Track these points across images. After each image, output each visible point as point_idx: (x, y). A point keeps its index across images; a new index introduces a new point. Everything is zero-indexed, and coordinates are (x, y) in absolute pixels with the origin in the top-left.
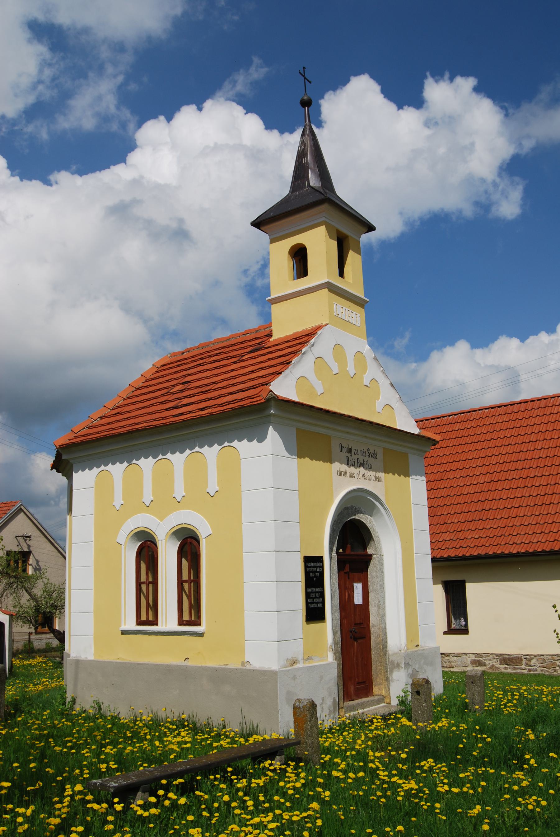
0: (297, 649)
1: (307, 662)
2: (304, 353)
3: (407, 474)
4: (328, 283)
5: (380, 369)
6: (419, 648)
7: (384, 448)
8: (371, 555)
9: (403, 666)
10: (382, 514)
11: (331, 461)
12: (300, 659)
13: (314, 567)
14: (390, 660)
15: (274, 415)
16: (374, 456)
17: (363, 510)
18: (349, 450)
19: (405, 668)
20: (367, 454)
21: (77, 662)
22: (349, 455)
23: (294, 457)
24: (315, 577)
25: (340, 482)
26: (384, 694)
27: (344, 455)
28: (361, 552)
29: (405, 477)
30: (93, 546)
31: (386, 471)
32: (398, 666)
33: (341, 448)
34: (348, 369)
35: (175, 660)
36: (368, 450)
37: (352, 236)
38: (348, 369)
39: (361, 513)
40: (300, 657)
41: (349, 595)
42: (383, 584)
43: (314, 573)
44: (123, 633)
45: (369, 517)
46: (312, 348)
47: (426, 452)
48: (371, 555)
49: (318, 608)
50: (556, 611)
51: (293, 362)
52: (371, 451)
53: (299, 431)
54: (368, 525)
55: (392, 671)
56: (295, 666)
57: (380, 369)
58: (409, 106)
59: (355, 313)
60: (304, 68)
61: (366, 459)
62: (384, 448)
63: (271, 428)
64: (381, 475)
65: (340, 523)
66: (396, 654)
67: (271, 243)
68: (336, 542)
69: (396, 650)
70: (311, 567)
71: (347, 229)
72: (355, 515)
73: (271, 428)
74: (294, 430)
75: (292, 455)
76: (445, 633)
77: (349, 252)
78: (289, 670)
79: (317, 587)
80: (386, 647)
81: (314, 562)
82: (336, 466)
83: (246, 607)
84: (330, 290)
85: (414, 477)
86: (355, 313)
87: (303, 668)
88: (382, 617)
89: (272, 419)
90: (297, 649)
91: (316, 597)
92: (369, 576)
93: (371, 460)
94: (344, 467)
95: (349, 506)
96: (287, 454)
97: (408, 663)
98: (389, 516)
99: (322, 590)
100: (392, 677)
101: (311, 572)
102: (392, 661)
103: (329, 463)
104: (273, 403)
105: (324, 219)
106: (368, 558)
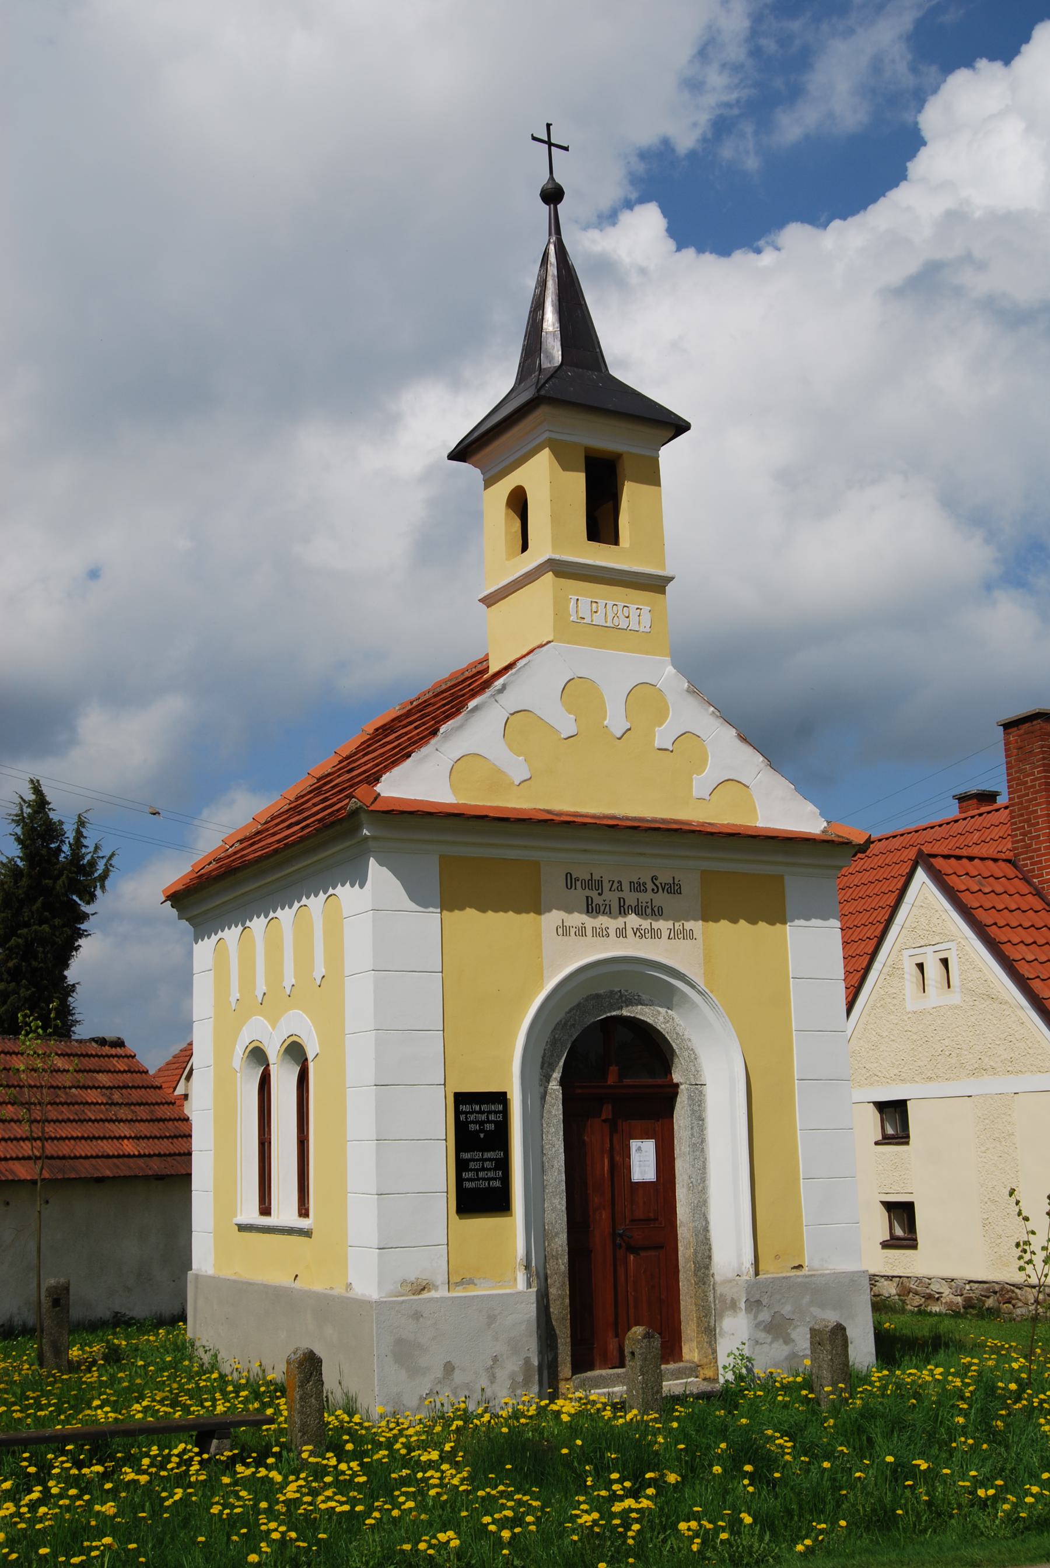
0: (432, 1263)
1: (461, 1288)
2: (476, 708)
3: (778, 916)
4: (550, 561)
5: (707, 710)
6: (805, 1271)
7: (703, 872)
8: (677, 1085)
9: (743, 1306)
10: (693, 1003)
11: (538, 908)
12: (439, 1283)
13: (481, 1112)
14: (718, 1292)
15: (374, 838)
16: (673, 888)
17: (644, 997)
18: (596, 885)
19: (748, 1309)
20: (650, 886)
21: (197, 1276)
22: (594, 894)
23: (431, 909)
24: (481, 1131)
25: (562, 948)
26: (696, 1360)
27: (580, 894)
28: (659, 1081)
29: (772, 923)
30: (212, 1074)
31: (707, 916)
32: (734, 1306)
33: (571, 881)
34: (606, 723)
35: (280, 1278)
36: (654, 879)
37: (634, 450)
38: (606, 723)
39: (640, 1002)
40: (441, 1278)
41: (612, 1164)
42: (703, 1141)
43: (482, 1123)
44: (242, 1228)
45: (663, 1010)
46: (499, 697)
47: (841, 868)
48: (677, 1085)
49: (490, 1190)
50: (1018, 1203)
51: (441, 731)
52: (664, 878)
53: (447, 864)
54: (661, 1026)
55: (722, 1317)
56: (425, 1295)
57: (707, 710)
58: (992, 59)
59: (633, 607)
60: (548, 126)
61: (644, 897)
62: (703, 872)
63: (372, 860)
64: (696, 926)
65: (573, 1026)
66: (730, 1281)
67: (486, 488)
68: (561, 1063)
69: (731, 1275)
70: (472, 1113)
71: (606, 438)
72: (621, 1008)
73: (372, 861)
74: (436, 858)
75: (426, 907)
76: (885, 1245)
77: (623, 485)
78: (403, 1302)
79: (489, 1151)
80: (707, 1267)
81: (480, 1103)
82: (554, 917)
83: (350, 1187)
84: (558, 574)
85: (797, 922)
86: (633, 607)
87: (443, 1299)
88: (701, 1206)
89: (371, 844)
90: (432, 1263)
91: (483, 1169)
92: (676, 1127)
93: (661, 899)
94: (578, 919)
95: (601, 992)
96: (413, 906)
97: (758, 1302)
98: (713, 1007)
99: (501, 1154)
100: (721, 1329)
101: (472, 1122)
102: (721, 1295)
103: (532, 915)
104: (363, 817)
105: (547, 435)
106: (672, 1092)
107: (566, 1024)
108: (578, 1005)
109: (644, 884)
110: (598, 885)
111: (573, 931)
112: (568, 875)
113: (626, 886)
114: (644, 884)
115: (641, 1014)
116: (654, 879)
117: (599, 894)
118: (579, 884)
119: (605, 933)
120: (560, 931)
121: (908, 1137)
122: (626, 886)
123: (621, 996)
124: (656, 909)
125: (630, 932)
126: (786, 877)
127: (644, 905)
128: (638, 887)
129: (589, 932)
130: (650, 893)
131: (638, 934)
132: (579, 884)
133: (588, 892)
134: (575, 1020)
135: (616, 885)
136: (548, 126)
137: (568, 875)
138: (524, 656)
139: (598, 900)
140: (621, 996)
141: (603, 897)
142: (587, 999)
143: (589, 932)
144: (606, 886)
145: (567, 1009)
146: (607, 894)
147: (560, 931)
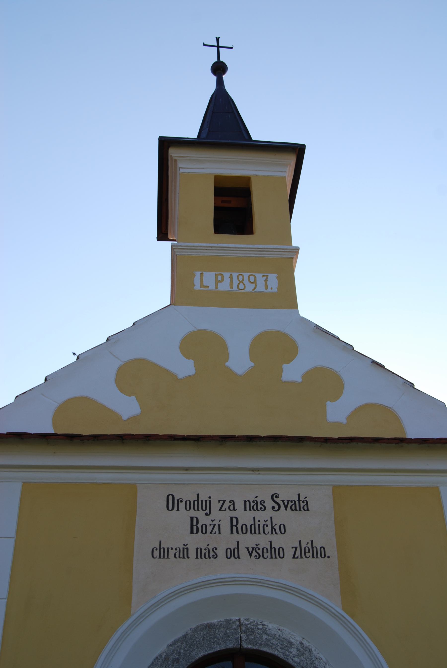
7: (336, 488)
20: (269, 504)
22: (200, 515)
52: (287, 494)
65: (177, 660)
74: (18, 486)
95: (215, 621)
107: (167, 659)
108: (185, 636)
109: (262, 502)
110: (206, 506)
111: (172, 553)
112: (170, 498)
113: (239, 505)
114: (262, 502)
115: (266, 645)
116: (274, 497)
117: (206, 514)
118: (182, 505)
119: (212, 553)
120: (156, 553)
121: (172, 246)
122: (239, 505)
123: (240, 626)
124: (277, 528)
125: (243, 552)
126: (442, 489)
127: (262, 523)
128: (255, 505)
129: (192, 553)
130: (269, 513)
131: (254, 554)
132: (182, 505)
133: (193, 513)
134: (179, 654)
135: (226, 505)
136: (205, 45)
137: (170, 498)
138: (318, 485)
139: (203, 520)
140: (240, 626)
141: (211, 517)
142: (196, 630)
143: (192, 553)
144: (215, 506)
145: (170, 641)
146: (216, 514)
147: (156, 553)
